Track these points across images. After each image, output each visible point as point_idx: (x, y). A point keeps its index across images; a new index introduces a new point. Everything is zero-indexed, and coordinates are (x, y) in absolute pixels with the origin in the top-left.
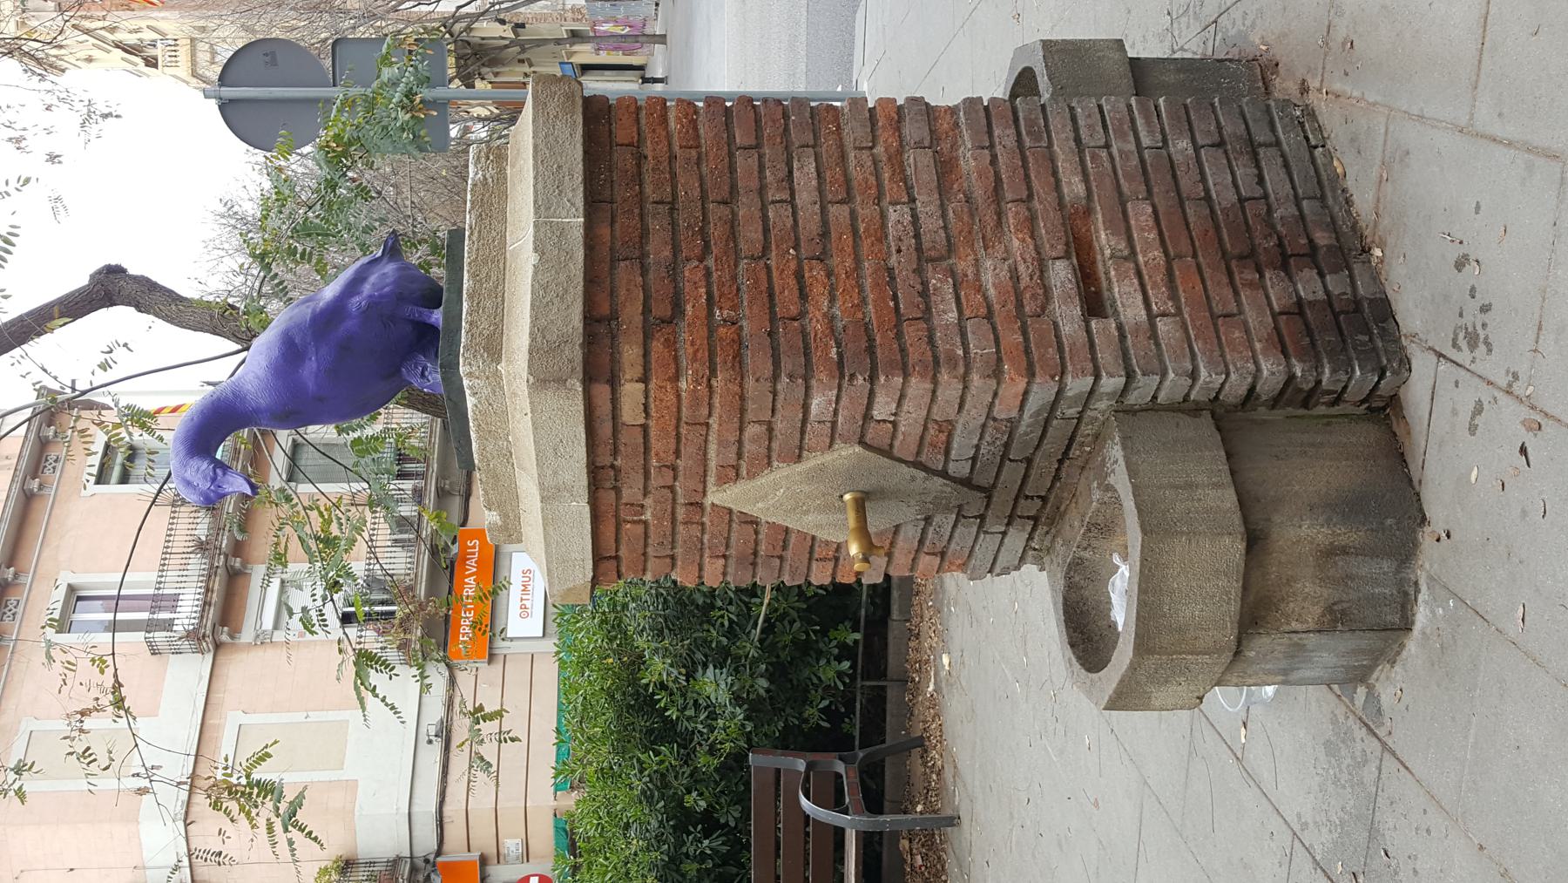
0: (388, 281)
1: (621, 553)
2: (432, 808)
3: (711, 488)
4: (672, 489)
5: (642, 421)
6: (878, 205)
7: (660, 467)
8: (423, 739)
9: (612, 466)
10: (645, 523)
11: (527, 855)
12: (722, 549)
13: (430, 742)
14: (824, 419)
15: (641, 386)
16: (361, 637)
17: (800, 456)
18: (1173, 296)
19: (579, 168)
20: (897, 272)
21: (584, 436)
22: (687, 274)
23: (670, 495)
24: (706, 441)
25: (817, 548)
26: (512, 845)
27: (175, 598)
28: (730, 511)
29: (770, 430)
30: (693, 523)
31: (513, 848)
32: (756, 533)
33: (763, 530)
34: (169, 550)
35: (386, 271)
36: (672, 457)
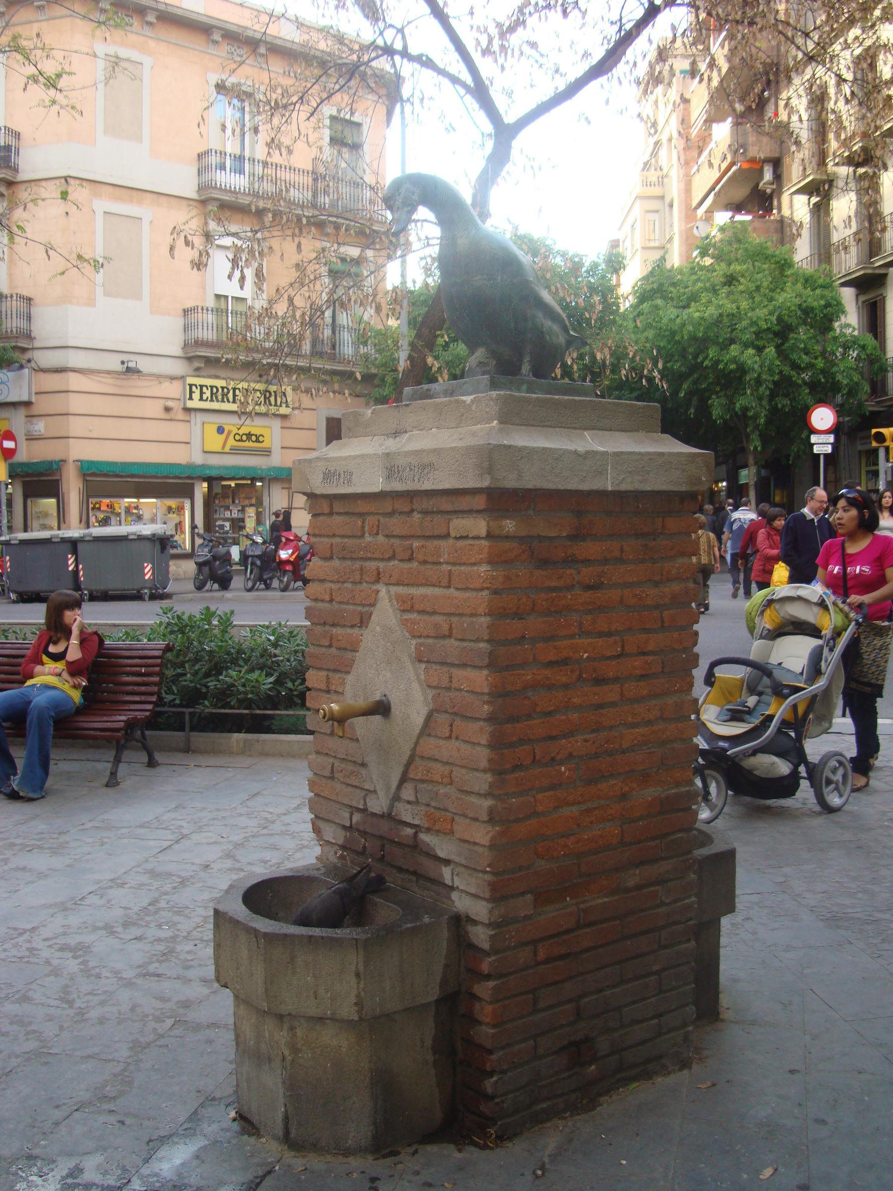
0: (554, 338)
1: (335, 517)
2: (71, 364)
3: (394, 589)
4: (393, 557)
5: (453, 534)
6: (620, 724)
7: (412, 549)
8: (125, 357)
9: (412, 511)
10: (362, 536)
11: (31, 438)
12: (338, 599)
13: (123, 363)
14: (454, 681)
15: (483, 533)
16: (207, 310)
17: (420, 661)
18: (548, 961)
19: (648, 488)
20: (570, 739)
21: (440, 488)
22: (568, 572)
23: (387, 556)
24: (434, 585)
25: (339, 675)
26: (40, 427)
27: (241, 172)
28: (373, 605)
29: (444, 637)
30: (361, 575)
31: (37, 428)
32: (352, 626)
33: (356, 631)
34: (278, 168)
35: (561, 337)
36: (421, 557)
